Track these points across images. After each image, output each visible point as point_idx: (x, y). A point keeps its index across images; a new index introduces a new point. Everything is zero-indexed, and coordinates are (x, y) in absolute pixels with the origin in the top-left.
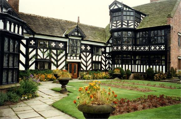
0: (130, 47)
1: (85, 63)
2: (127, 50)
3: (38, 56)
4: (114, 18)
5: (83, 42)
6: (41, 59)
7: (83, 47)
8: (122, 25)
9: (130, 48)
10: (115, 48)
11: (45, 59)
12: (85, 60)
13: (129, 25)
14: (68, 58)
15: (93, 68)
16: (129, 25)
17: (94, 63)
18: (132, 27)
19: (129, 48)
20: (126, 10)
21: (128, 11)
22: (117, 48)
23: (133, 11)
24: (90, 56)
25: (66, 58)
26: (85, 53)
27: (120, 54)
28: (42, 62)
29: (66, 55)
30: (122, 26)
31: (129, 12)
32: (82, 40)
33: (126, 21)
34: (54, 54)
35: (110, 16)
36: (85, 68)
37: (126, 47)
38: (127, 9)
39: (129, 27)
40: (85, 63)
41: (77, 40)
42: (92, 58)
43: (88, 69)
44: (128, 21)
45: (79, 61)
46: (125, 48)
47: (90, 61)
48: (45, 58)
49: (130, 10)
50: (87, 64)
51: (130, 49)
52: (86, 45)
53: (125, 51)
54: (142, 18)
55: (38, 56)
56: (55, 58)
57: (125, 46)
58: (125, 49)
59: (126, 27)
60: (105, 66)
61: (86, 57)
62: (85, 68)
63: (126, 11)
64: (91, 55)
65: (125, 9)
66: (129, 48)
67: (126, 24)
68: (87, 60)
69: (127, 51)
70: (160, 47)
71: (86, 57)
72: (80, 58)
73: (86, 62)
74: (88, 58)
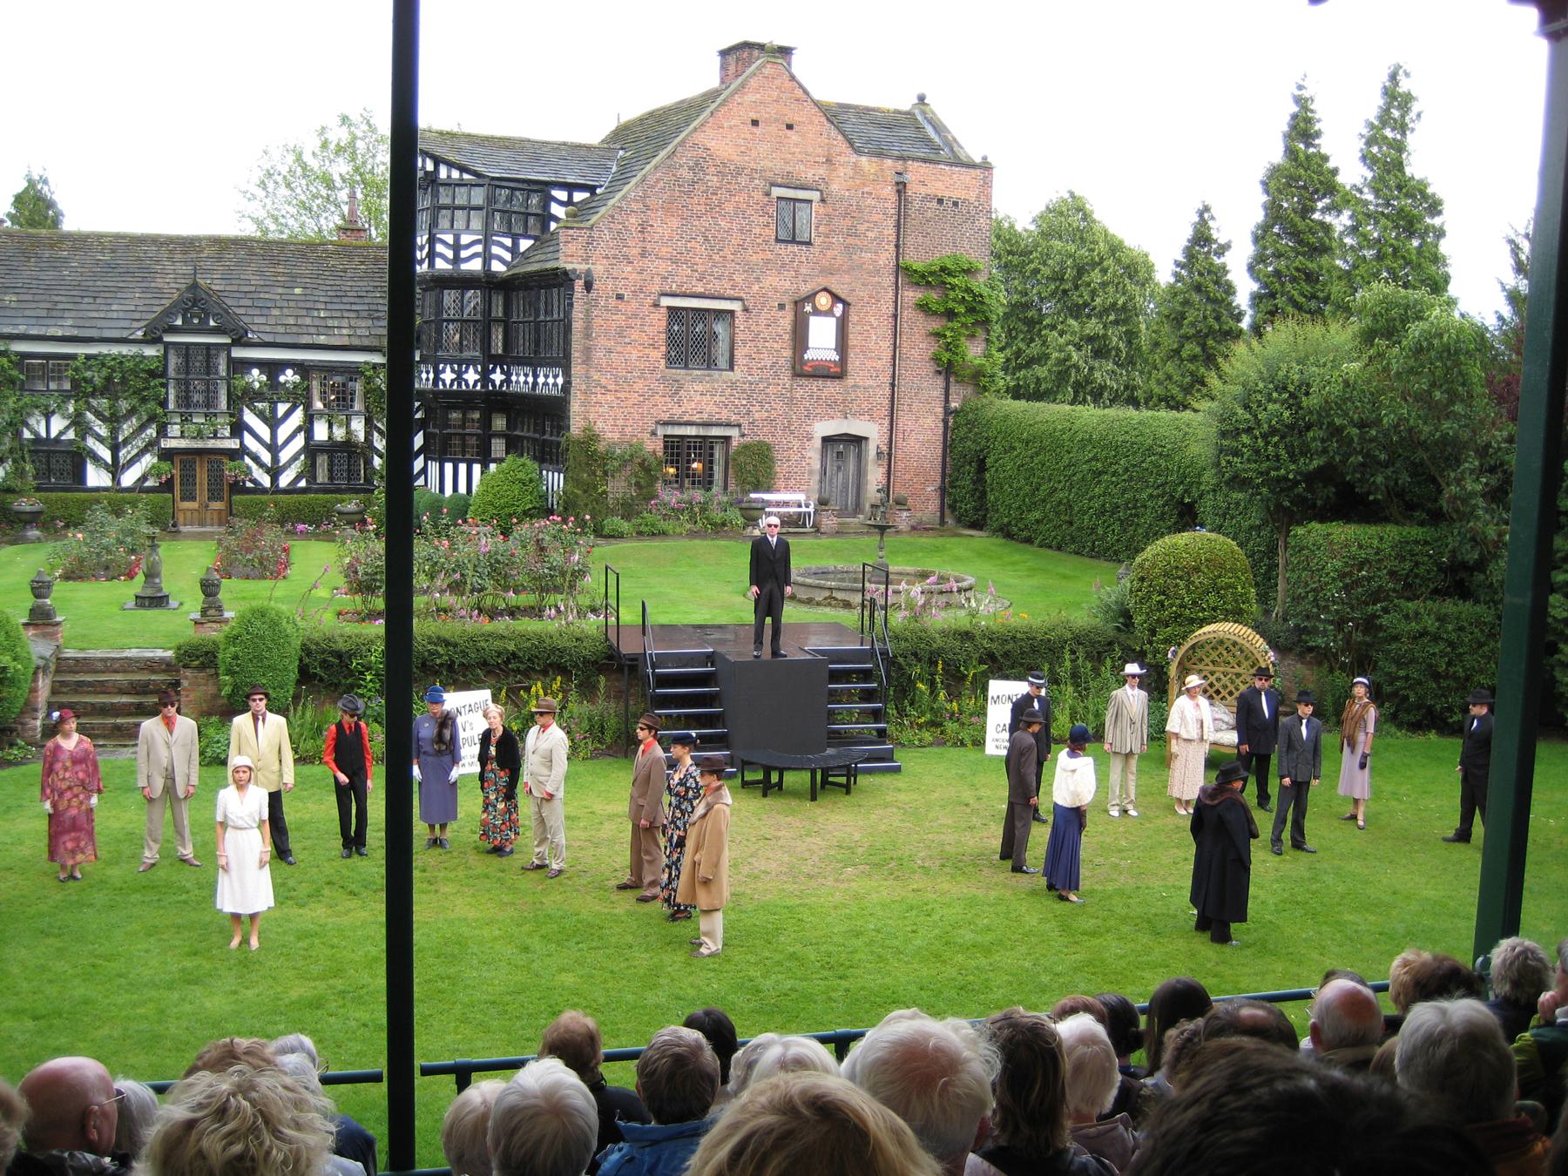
0: (471, 369)
1: (266, 457)
2: (459, 385)
3: (288, 406)
4: (444, 212)
5: (238, 353)
6: (37, 440)
7: (256, 377)
8: (487, 257)
9: (471, 376)
10: (448, 376)
11: (57, 440)
12: (268, 439)
13: (479, 248)
14: (174, 430)
15: (315, 478)
16: (464, 254)
17: (323, 451)
18: (476, 265)
19: (465, 376)
20: (449, 177)
21: (461, 184)
22: (459, 378)
23: (480, 181)
24: (297, 417)
25: (162, 432)
26: (103, 403)
27: (410, 412)
28: (43, 451)
29: (309, 419)
30: (431, 264)
31: (463, 189)
32: (240, 342)
33: (508, 242)
34: (98, 414)
35: (1542, 47)
36: (266, 481)
37: (453, 371)
38: (455, 174)
39: (464, 267)
40: (266, 457)
41: (208, 346)
42: (307, 428)
43: (284, 481)
44: (457, 238)
45: (233, 444)
46: (448, 376)
47: (299, 441)
48: (53, 434)
49: (466, 176)
50: (275, 459)
51: (471, 383)
52: (273, 368)
53: (448, 394)
54: (557, 210)
55: (288, 406)
56: (264, 431)
57: (451, 364)
58: (471, 383)
59: (450, 267)
60: (268, 471)
61: (273, 423)
62: (266, 481)
63: (450, 185)
64: (305, 415)
65: (443, 172)
66: (465, 376)
67: (450, 254)
68: (280, 441)
69: (459, 394)
70: (459, 374)
71: (273, 423)
72: (238, 428)
73: (274, 448)
74: (284, 432)
